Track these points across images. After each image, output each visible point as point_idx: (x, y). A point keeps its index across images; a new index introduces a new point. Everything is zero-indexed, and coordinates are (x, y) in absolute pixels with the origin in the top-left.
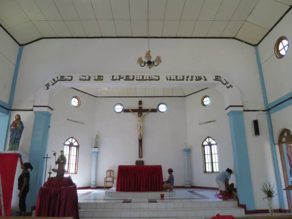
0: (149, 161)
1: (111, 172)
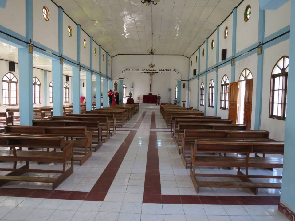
0: (154, 93)
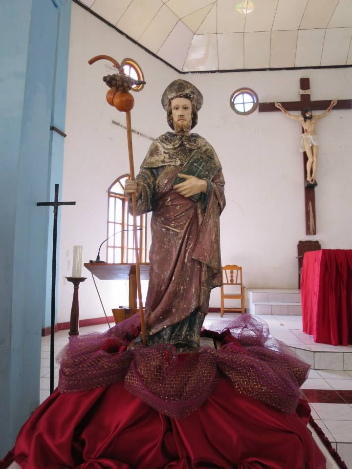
1: (235, 271)
